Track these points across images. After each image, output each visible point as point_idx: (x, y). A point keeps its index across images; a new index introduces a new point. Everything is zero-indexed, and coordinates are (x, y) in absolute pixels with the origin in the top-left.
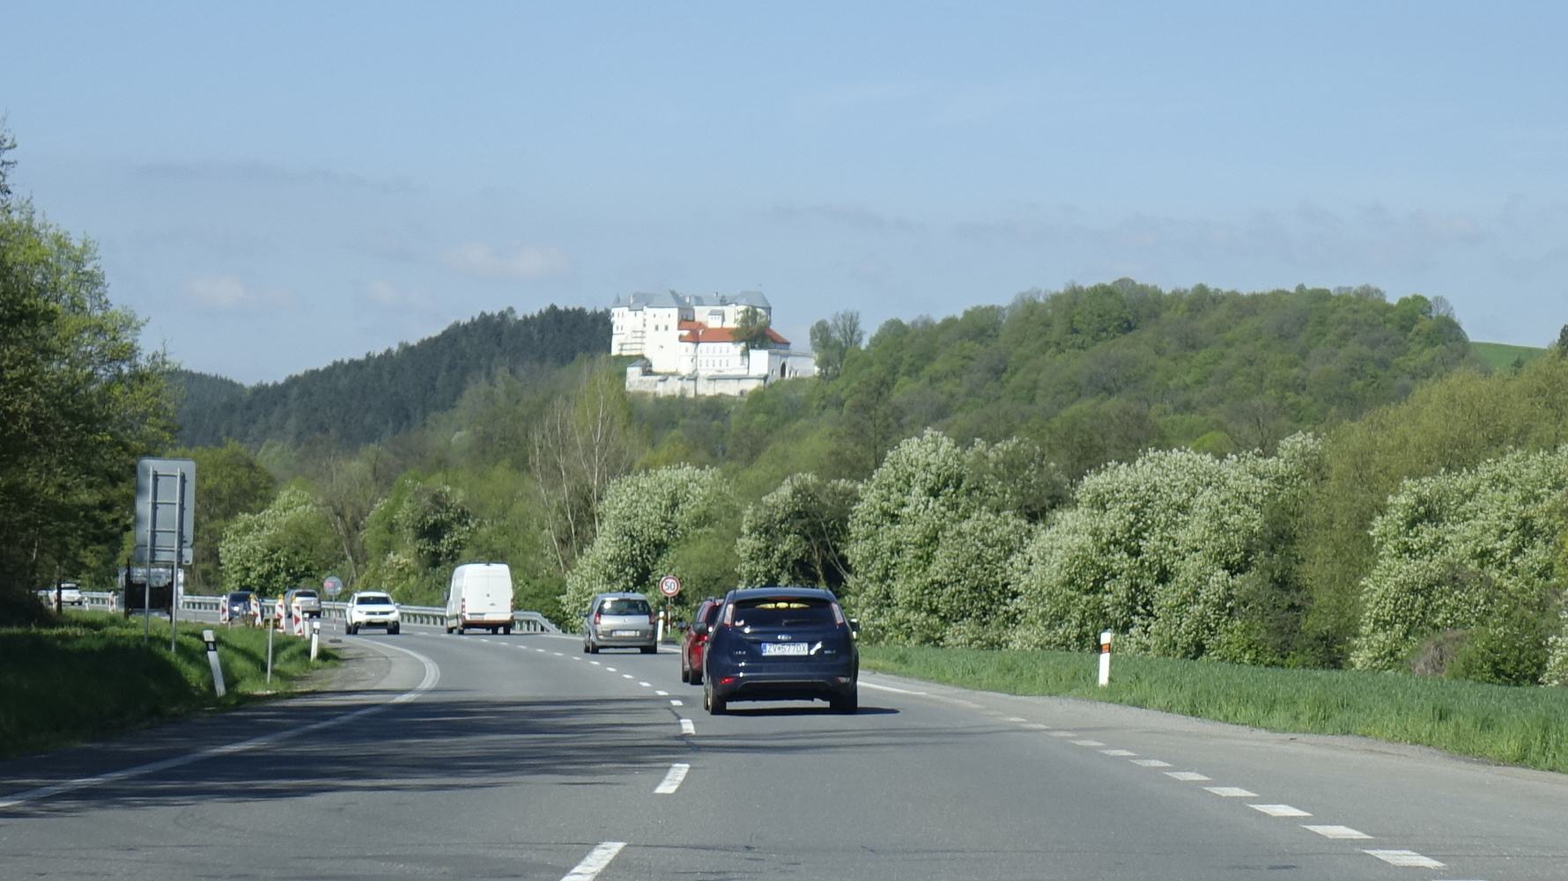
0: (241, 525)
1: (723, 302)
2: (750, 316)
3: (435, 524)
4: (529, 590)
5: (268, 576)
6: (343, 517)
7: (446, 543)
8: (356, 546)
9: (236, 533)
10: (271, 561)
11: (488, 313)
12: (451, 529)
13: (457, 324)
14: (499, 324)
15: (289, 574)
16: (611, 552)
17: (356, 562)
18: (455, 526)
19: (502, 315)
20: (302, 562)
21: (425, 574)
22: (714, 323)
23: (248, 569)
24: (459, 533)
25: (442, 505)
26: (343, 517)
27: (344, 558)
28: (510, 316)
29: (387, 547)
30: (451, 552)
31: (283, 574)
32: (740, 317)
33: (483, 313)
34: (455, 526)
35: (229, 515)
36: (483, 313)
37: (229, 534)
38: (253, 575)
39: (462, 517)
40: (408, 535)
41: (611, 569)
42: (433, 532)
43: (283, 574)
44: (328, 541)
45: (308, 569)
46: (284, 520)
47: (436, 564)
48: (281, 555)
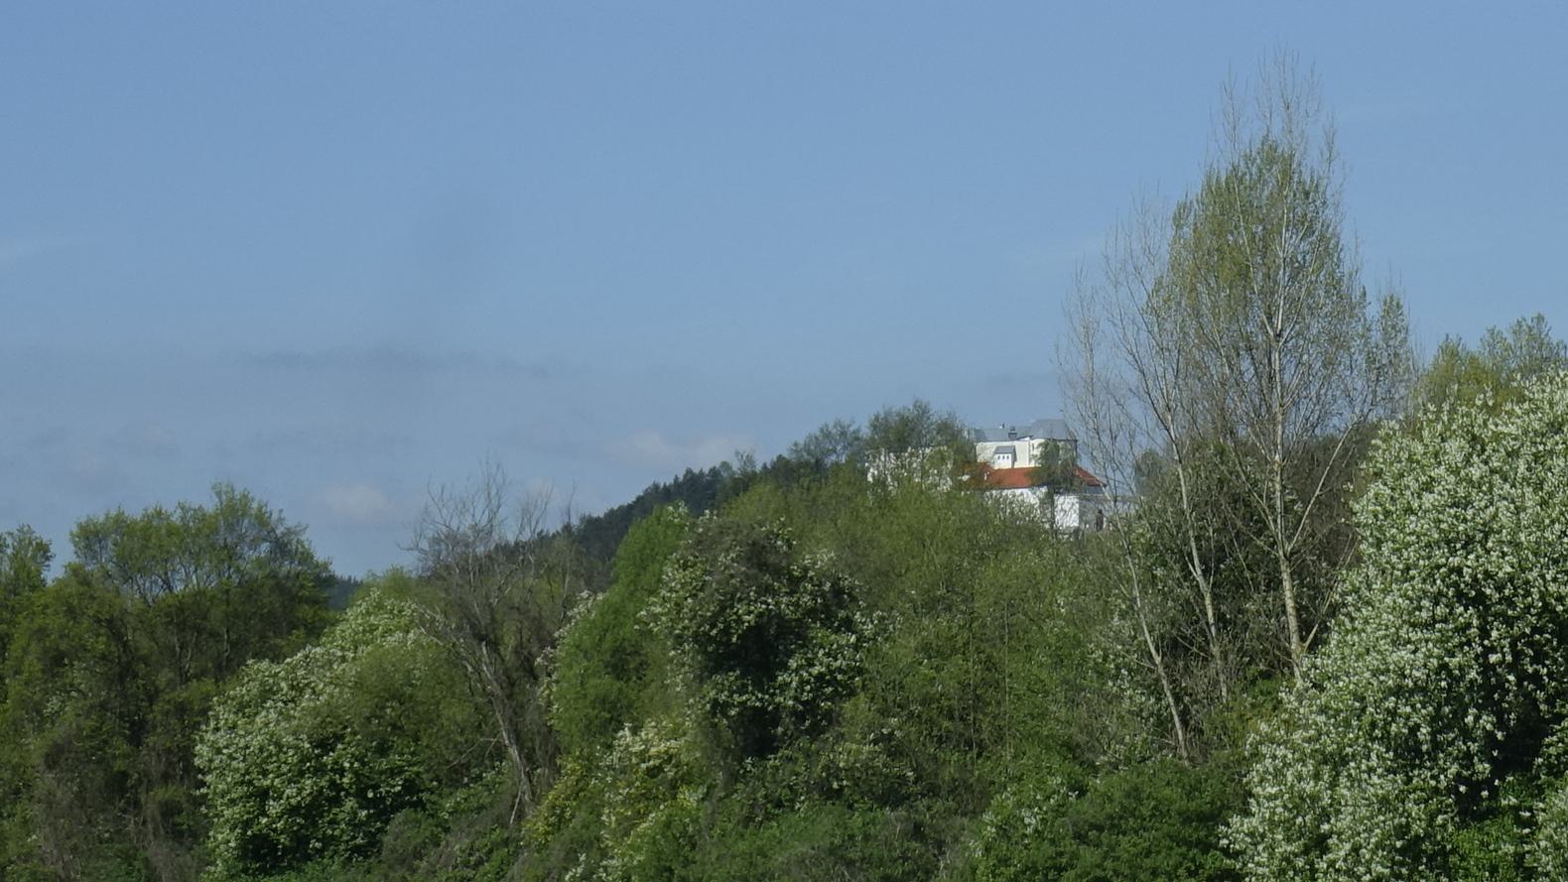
0: (254, 688)
1: (1013, 435)
2: (1050, 452)
3: (757, 630)
4: (1087, 809)
5: (310, 812)
6: (494, 645)
7: (792, 679)
8: (530, 716)
9: (241, 708)
10: (319, 770)
11: (696, 471)
12: (804, 641)
13: (656, 487)
14: (710, 485)
15: (365, 803)
16: (1415, 659)
17: (529, 758)
18: (818, 632)
19: (714, 472)
20: (394, 772)
21: (734, 777)
22: (1003, 463)
23: (263, 795)
24: (829, 651)
25: (777, 573)
26: (494, 645)
27: (500, 753)
28: (725, 474)
29: (612, 716)
30: (811, 706)
31: (350, 804)
32: (1037, 452)
33: (689, 472)
34: (818, 632)
35: (226, 668)
36: (689, 472)
37: (225, 714)
38: (274, 807)
39: (834, 606)
40: (677, 673)
41: (1417, 715)
42: (753, 652)
43: (350, 804)
44: (456, 712)
45: (410, 787)
46: (351, 670)
47: (763, 746)
48: (343, 755)
